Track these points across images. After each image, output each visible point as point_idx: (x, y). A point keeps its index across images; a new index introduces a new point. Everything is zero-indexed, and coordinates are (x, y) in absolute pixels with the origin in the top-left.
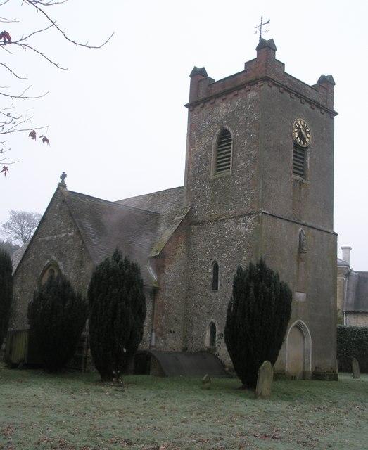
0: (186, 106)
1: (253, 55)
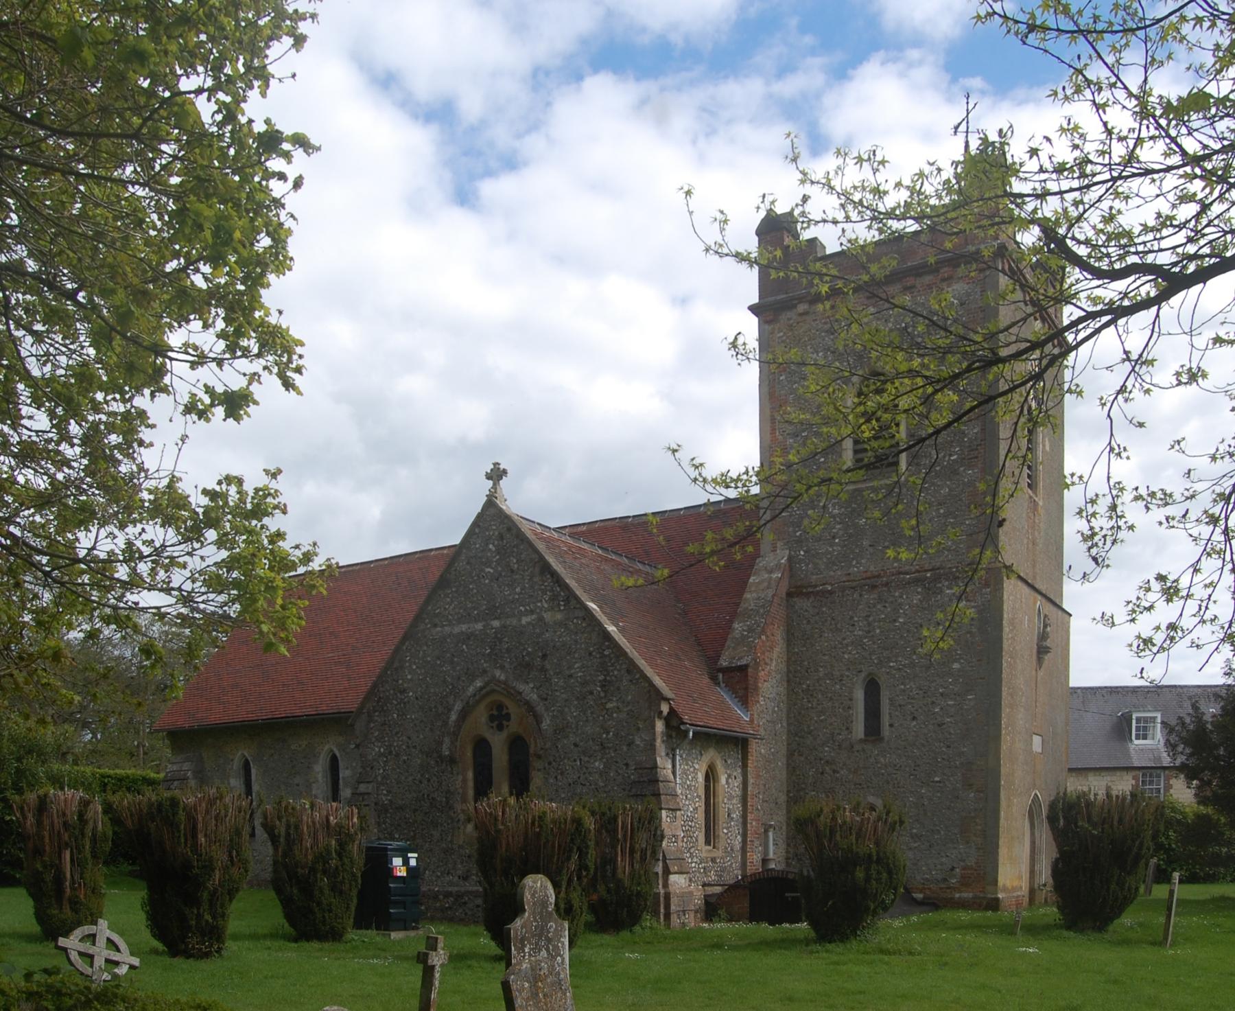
0: (753, 309)
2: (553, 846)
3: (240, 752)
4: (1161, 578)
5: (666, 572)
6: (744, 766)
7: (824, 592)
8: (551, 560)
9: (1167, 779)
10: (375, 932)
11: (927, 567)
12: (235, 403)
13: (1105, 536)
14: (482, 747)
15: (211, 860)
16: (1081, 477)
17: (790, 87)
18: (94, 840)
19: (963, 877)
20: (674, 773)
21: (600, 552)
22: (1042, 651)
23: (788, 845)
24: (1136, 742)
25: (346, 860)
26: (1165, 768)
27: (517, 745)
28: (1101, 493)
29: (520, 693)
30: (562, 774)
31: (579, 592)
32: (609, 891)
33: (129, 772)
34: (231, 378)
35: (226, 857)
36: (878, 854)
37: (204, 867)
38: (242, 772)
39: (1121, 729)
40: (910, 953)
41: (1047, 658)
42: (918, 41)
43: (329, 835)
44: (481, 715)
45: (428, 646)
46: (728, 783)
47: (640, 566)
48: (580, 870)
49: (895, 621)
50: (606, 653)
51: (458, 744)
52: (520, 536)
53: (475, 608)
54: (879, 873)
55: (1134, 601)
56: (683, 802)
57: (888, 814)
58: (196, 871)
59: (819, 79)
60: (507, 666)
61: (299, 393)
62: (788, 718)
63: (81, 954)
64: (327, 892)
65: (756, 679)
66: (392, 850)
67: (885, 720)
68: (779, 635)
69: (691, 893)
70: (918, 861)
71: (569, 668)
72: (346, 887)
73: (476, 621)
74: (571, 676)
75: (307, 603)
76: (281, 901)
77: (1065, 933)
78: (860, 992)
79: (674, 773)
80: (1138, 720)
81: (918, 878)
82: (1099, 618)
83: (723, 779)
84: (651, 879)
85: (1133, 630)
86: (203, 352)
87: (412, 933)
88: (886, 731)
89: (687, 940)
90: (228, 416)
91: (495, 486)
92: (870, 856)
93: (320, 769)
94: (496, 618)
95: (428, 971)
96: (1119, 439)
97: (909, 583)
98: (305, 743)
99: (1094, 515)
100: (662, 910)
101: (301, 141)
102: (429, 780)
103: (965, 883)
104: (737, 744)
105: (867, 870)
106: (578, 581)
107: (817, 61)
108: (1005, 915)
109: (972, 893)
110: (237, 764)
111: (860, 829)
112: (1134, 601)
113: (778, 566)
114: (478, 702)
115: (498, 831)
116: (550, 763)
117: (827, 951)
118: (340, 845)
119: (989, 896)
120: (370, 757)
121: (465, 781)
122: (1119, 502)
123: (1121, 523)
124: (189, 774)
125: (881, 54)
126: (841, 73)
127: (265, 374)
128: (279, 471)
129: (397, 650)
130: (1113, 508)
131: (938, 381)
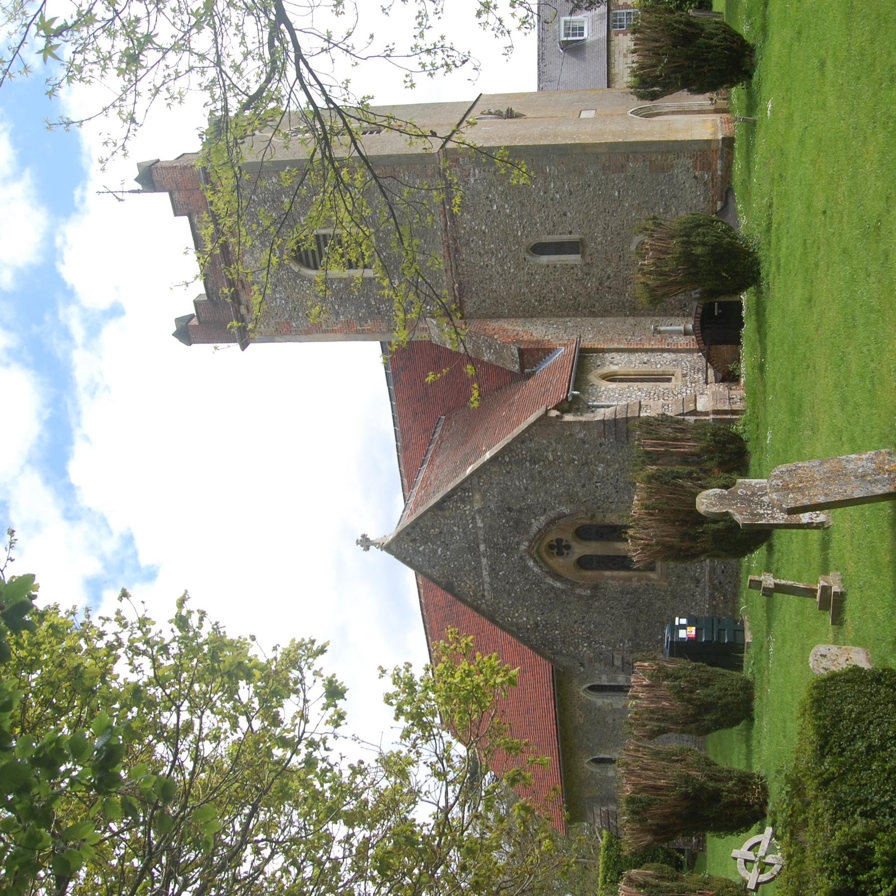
0: (243, 347)
1: (163, 198)
2: (672, 499)
3: (586, 765)
4: (479, 14)
5: (469, 367)
6: (603, 351)
7: (460, 290)
8: (432, 502)
9: (619, 7)
10: (745, 654)
11: (442, 209)
12: (334, 692)
13: (448, 56)
14: (584, 563)
15: (680, 776)
16: (407, 76)
17: (78, 331)
18: (662, 878)
19: (703, 169)
20: (608, 407)
21: (425, 466)
22: (510, 115)
23: (672, 315)
24: (586, 35)
25: (681, 674)
26: (609, 10)
27: (583, 534)
28: (419, 61)
29: (540, 530)
30: (608, 498)
31: (458, 480)
32: (712, 459)
33: (601, 861)
34: (316, 692)
35: (678, 765)
36: (682, 236)
37: (686, 782)
38: (603, 765)
39: (574, 48)
40: (771, 206)
41: (515, 110)
42: (49, 237)
43: (659, 686)
44: (557, 562)
45: (500, 603)
46: (618, 364)
47: (437, 435)
48: (691, 478)
49: (484, 232)
50: (507, 460)
51: (581, 582)
52: (414, 525)
53: (470, 564)
54: (698, 235)
55: (495, 32)
56: (633, 400)
57: (647, 230)
58: (690, 790)
59: (73, 309)
60: (517, 539)
61: (328, 643)
62: (562, 316)
63: (762, 872)
64: (708, 691)
65: (530, 342)
66: (672, 637)
67: (566, 238)
68: (494, 325)
69: (713, 393)
70: (690, 201)
71: (519, 489)
72: (705, 676)
73: (480, 563)
74: (526, 489)
75: (478, 653)
76: (716, 729)
77: (755, 79)
78: (805, 243)
79: (608, 407)
80: (567, 35)
81: (703, 206)
82: (506, 57)
83: (614, 368)
84: (703, 425)
85: (515, 33)
86: (298, 713)
87: (747, 625)
88: (575, 237)
89: (756, 396)
90: (343, 697)
91: (374, 544)
92: (683, 242)
93: (600, 701)
94: (478, 547)
95: (778, 588)
96: (381, 51)
97: (454, 222)
98: (578, 711)
99: (432, 65)
100: (729, 417)
101: (181, 602)
102: (612, 608)
103: (708, 166)
104: (583, 359)
105: (695, 244)
106: (449, 481)
107: (61, 312)
108: (737, 131)
109: (715, 162)
110: (596, 769)
111: (660, 251)
112: (495, 32)
113: (438, 326)
114: (546, 564)
115: (658, 543)
116: (599, 508)
117: (767, 276)
118: (668, 677)
119: (720, 146)
120: (592, 655)
121: (613, 578)
122: (425, 48)
123: (439, 45)
124: (604, 809)
125: (58, 264)
126: (70, 295)
127: (313, 668)
128: (380, 667)
129: (503, 628)
130: (428, 51)
131: (337, 179)
